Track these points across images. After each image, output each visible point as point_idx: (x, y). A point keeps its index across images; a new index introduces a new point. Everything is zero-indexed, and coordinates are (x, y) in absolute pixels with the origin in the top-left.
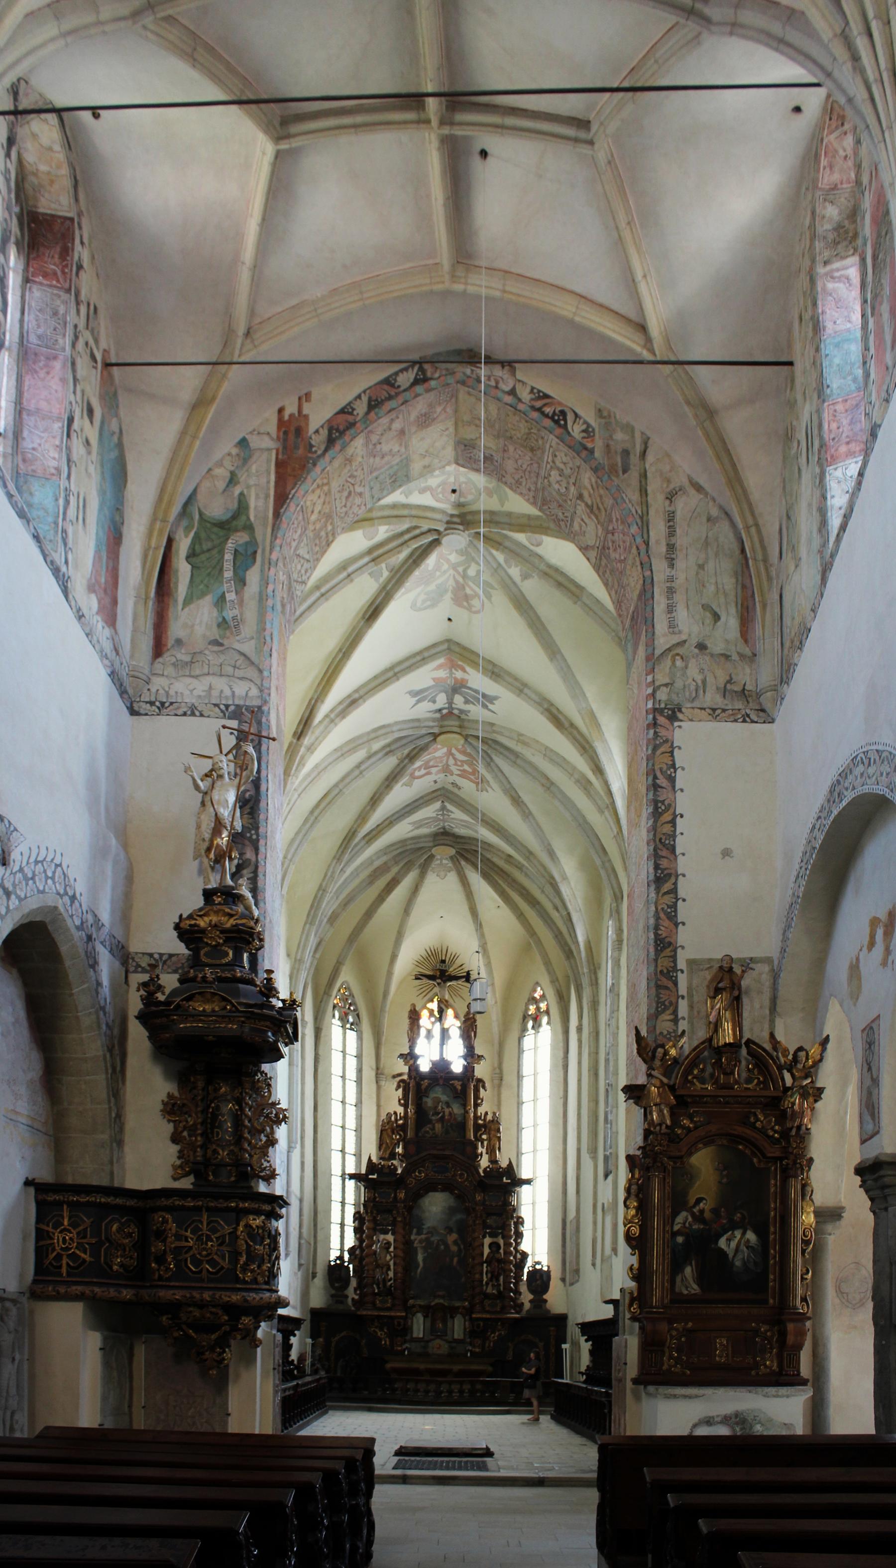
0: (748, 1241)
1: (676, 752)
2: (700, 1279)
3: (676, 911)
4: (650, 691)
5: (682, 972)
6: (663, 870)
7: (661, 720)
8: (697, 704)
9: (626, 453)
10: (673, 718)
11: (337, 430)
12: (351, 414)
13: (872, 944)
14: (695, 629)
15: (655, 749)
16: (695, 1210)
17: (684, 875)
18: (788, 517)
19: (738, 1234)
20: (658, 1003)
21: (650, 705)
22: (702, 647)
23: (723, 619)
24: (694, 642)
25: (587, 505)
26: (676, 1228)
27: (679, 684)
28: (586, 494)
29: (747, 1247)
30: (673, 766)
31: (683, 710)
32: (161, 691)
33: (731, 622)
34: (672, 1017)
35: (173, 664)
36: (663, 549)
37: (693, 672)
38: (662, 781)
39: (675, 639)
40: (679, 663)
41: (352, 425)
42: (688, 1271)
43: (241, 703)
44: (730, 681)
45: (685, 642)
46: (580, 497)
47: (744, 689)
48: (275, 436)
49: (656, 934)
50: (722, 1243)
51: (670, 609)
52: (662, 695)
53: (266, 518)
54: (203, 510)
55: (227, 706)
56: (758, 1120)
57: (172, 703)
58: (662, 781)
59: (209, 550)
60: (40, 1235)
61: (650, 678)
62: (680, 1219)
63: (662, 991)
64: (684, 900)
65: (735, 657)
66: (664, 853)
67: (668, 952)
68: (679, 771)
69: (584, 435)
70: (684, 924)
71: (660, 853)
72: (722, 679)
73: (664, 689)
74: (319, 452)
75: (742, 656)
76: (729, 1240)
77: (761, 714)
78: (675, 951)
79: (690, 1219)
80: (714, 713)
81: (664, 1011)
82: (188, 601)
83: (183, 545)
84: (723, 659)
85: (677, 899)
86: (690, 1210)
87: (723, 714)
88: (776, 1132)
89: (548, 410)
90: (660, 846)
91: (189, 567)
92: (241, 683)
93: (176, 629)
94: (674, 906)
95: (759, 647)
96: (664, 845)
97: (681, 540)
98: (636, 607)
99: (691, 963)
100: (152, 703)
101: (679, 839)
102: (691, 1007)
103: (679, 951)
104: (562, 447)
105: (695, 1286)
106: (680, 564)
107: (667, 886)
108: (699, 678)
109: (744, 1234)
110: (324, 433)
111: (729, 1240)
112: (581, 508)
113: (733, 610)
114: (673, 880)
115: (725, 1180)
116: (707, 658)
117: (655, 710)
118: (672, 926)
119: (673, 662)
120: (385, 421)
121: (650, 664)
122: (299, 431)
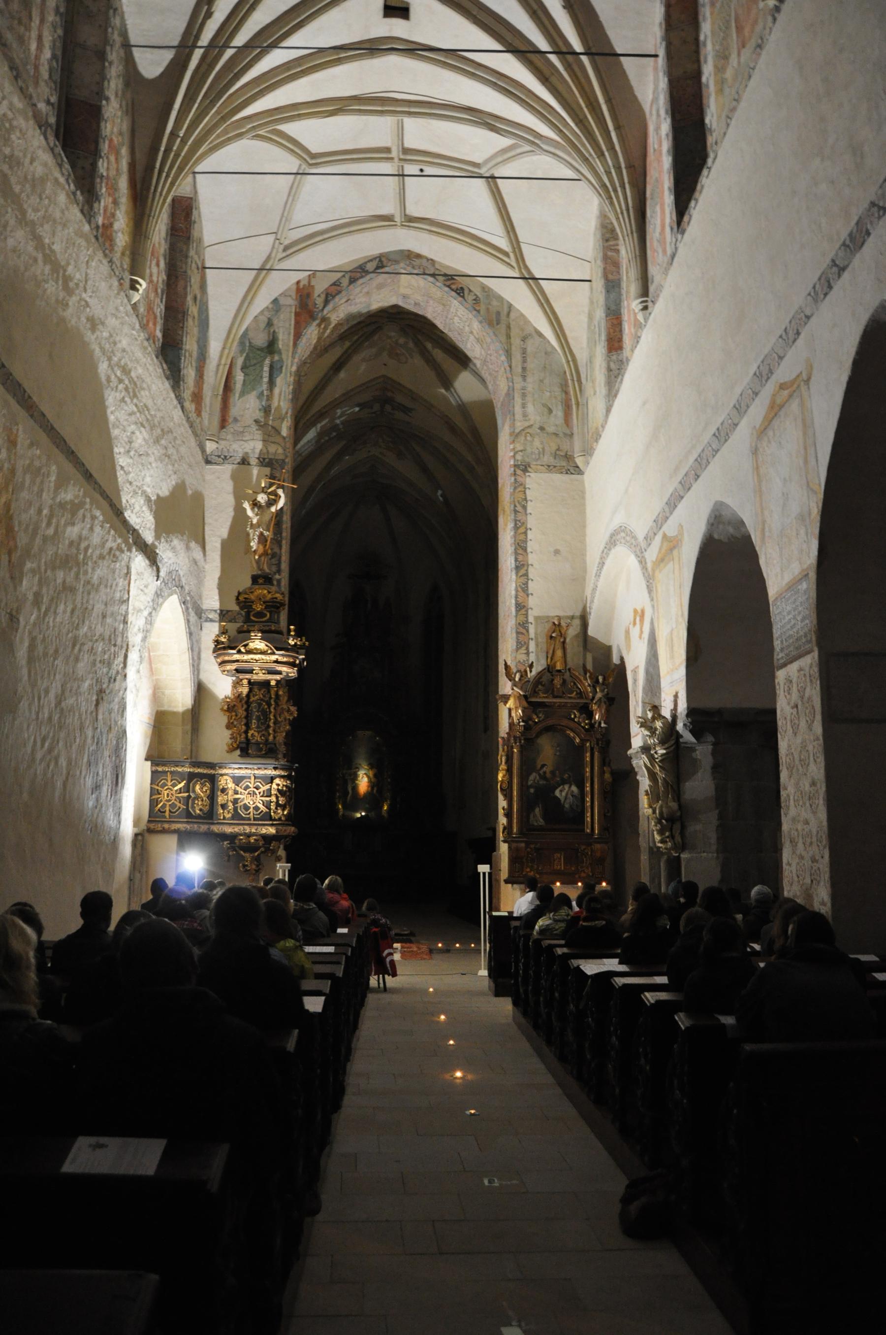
0: (573, 792)
1: (527, 491)
2: (545, 816)
3: (527, 587)
4: (512, 454)
5: (531, 623)
6: (520, 562)
7: (519, 472)
8: (539, 463)
9: (498, 313)
10: (525, 470)
11: (331, 295)
12: (339, 286)
13: (635, 624)
14: (538, 418)
15: (515, 488)
16: (541, 772)
17: (532, 565)
18: (591, 362)
19: (566, 787)
20: (517, 642)
21: (512, 463)
22: (542, 429)
23: (554, 412)
24: (537, 426)
25: (475, 337)
26: (530, 783)
27: (529, 450)
28: (475, 332)
29: (572, 796)
30: (526, 499)
31: (532, 466)
32: (225, 450)
33: (559, 413)
34: (525, 651)
35: (233, 433)
36: (520, 370)
37: (537, 443)
38: (519, 508)
39: (527, 424)
40: (529, 438)
41: (340, 292)
42: (537, 810)
43: (272, 457)
44: (558, 449)
45: (532, 425)
46: (471, 333)
47: (566, 454)
48: (294, 297)
49: (516, 601)
50: (557, 793)
51: (524, 406)
52: (519, 457)
53: (288, 346)
54: (252, 341)
55: (264, 459)
56: (575, 716)
57: (231, 457)
58: (519, 508)
59: (255, 365)
60: (153, 792)
61: (512, 447)
62: (532, 777)
63: (520, 636)
64: (532, 580)
65: (561, 435)
66: (520, 551)
67: (523, 611)
68: (529, 503)
69: (474, 302)
70: (532, 594)
71: (518, 552)
72: (554, 447)
73: (520, 453)
74: (321, 308)
75: (565, 434)
76: (561, 791)
77: (577, 469)
78: (527, 611)
79: (538, 777)
80: (550, 468)
81: (521, 647)
82: (243, 393)
83: (240, 362)
84: (554, 436)
85: (528, 579)
86: (538, 772)
87: (554, 469)
88: (586, 724)
89: (454, 287)
90: (518, 548)
91: (243, 374)
92: (273, 445)
93: (234, 411)
94: (526, 584)
95: (575, 429)
96: (521, 547)
97: (530, 365)
98: (504, 400)
99: (537, 618)
100: (219, 456)
101: (529, 544)
102: (537, 645)
103: (530, 612)
104: (461, 306)
105: (541, 820)
106: (530, 379)
107: (522, 572)
108: (540, 447)
109: (570, 787)
110: (323, 296)
111: (561, 791)
112: (472, 338)
113: (560, 407)
114: (525, 568)
115: (558, 754)
116: (545, 435)
117: (515, 466)
118: (526, 596)
119: (526, 437)
120: (358, 290)
121: (512, 438)
122: (308, 295)
